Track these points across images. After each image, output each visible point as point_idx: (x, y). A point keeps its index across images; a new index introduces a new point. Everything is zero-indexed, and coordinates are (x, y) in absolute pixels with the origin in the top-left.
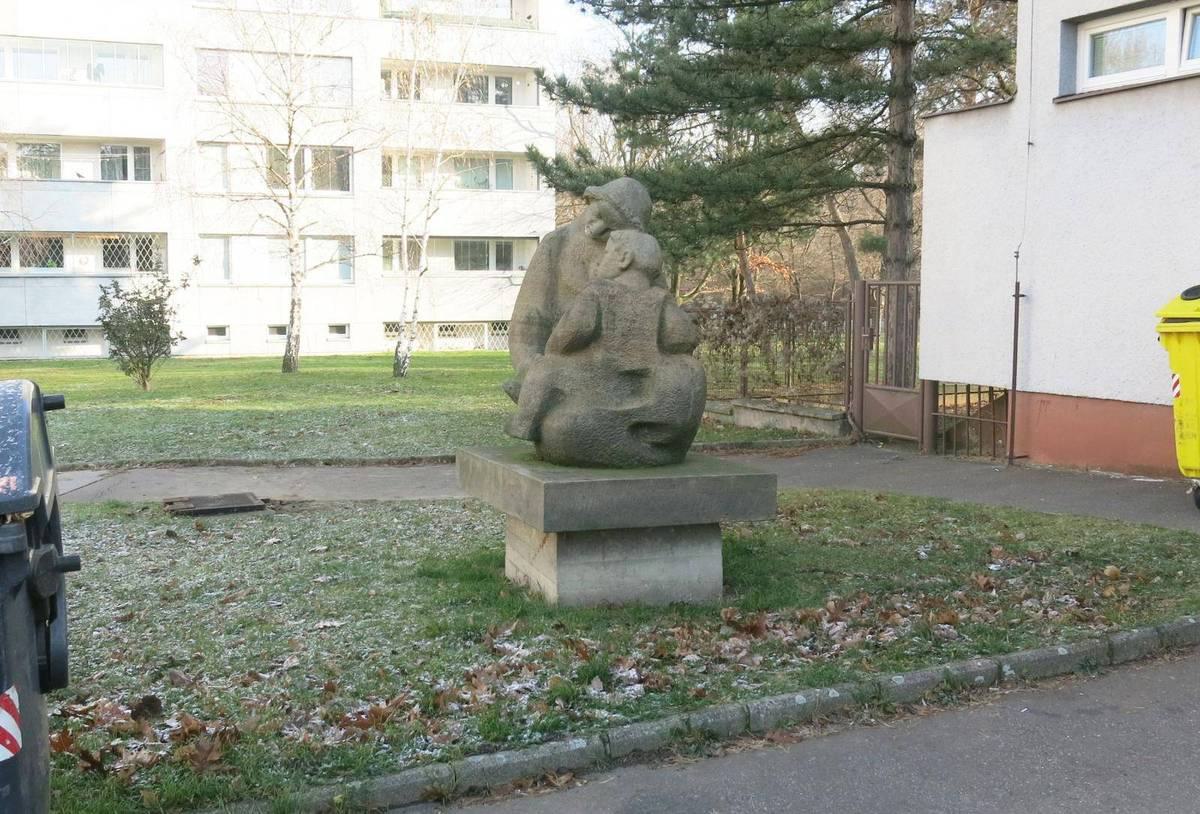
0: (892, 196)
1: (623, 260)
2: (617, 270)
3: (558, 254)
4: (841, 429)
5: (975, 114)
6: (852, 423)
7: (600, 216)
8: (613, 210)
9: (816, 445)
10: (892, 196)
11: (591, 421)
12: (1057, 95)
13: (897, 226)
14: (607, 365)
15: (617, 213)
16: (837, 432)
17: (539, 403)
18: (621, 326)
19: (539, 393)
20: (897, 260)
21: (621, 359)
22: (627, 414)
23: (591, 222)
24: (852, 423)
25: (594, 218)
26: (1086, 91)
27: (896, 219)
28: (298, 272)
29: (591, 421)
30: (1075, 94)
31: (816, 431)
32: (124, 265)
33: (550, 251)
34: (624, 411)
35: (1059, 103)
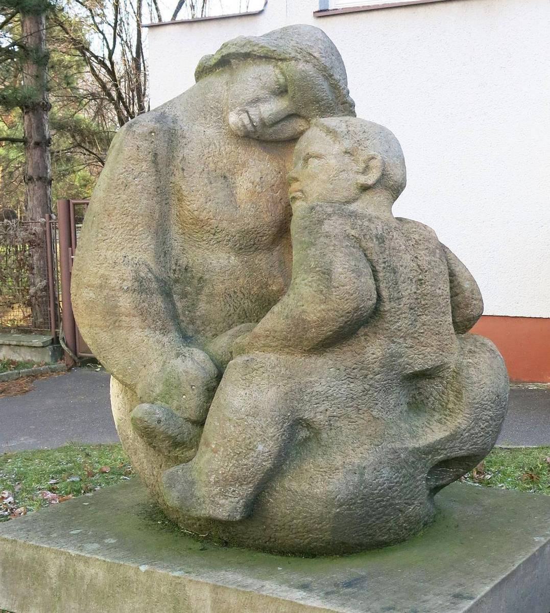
0: (30, 114)
1: (366, 170)
2: (354, 191)
3: (170, 161)
4: (52, 356)
5: (177, 27)
6: (66, 348)
7: (281, 91)
8: (320, 80)
9: (33, 376)
10: (30, 114)
11: (386, 472)
12: (317, 9)
13: (37, 144)
14: (390, 362)
15: (326, 86)
16: (48, 359)
17: (275, 450)
18: (407, 290)
19: (271, 431)
20: (40, 178)
21: (409, 351)
22: (431, 449)
23: (256, 101)
24: (66, 348)
25: (262, 93)
26: (340, 7)
27: (36, 138)
28: (103, 207)
29: (386, 472)
30: (328, 10)
31: (21, 359)
32: (109, 140)
33: (156, 155)
34: (428, 446)
35: (320, 17)
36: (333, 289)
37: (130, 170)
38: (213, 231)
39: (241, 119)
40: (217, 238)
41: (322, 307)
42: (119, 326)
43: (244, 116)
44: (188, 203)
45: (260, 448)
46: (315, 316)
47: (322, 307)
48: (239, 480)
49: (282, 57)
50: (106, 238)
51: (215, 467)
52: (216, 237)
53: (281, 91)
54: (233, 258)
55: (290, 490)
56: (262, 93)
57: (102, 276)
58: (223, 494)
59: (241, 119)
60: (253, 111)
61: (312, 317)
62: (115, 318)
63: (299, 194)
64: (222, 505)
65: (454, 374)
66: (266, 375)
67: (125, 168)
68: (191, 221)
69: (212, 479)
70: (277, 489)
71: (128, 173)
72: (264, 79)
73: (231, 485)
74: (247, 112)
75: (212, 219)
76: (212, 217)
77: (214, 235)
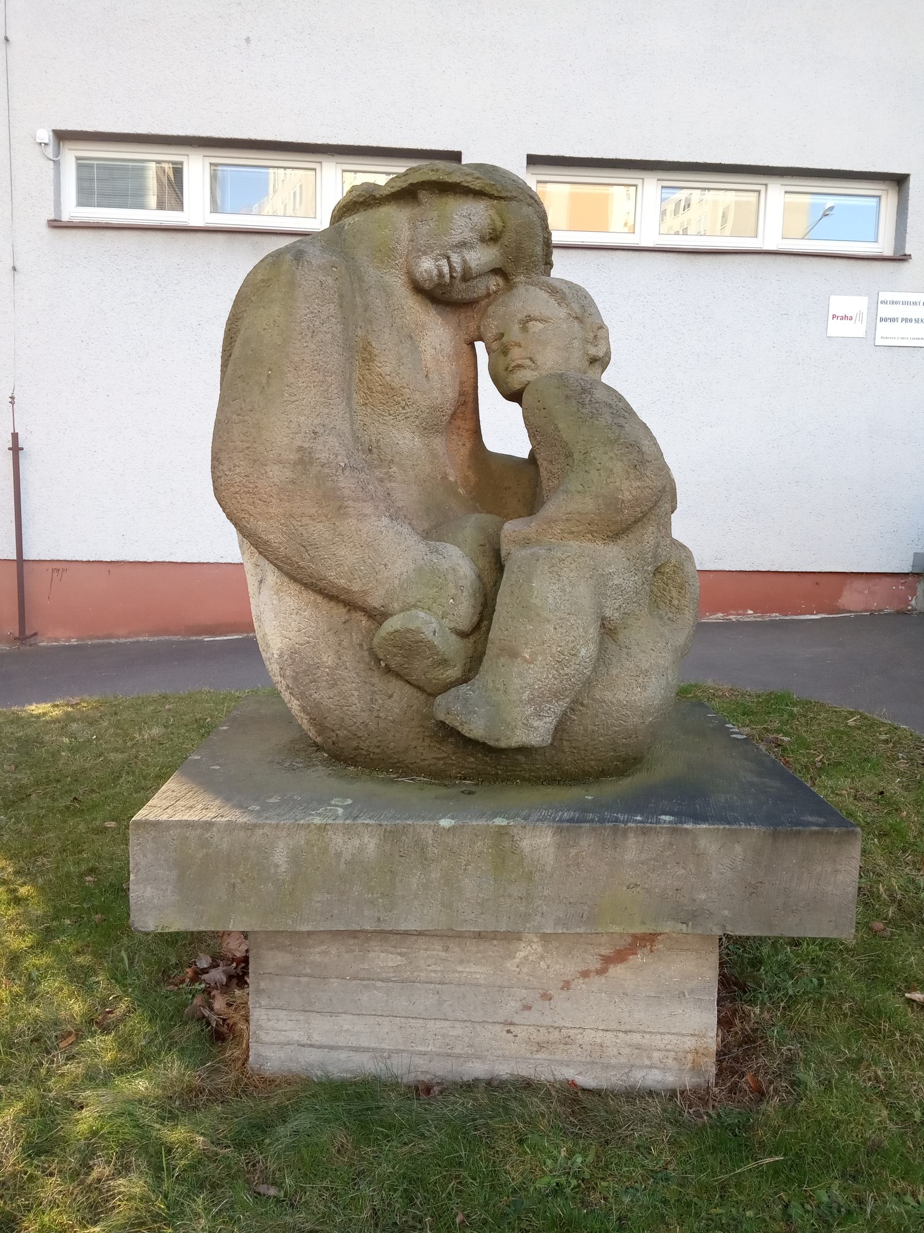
36: (647, 464)
37: (316, 311)
38: (403, 403)
39: (439, 268)
40: (407, 413)
41: (638, 484)
42: (345, 514)
43: (444, 262)
44: (380, 365)
45: (583, 652)
46: (631, 493)
47: (638, 484)
48: (557, 695)
49: (503, 194)
50: (294, 398)
51: (530, 681)
52: (404, 411)
53: (493, 238)
54: (417, 439)
55: (604, 702)
56: (468, 235)
57: (300, 449)
58: (538, 715)
59: (439, 268)
60: (455, 258)
61: (627, 495)
62: (339, 503)
63: (528, 362)
64: (536, 729)
65: (675, 569)
66: (573, 566)
67: (308, 308)
68: (379, 388)
69: (525, 697)
70: (585, 702)
71: (313, 315)
72: (475, 219)
73: (548, 702)
74: (448, 258)
75: (404, 388)
76: (405, 385)
77: (403, 408)
